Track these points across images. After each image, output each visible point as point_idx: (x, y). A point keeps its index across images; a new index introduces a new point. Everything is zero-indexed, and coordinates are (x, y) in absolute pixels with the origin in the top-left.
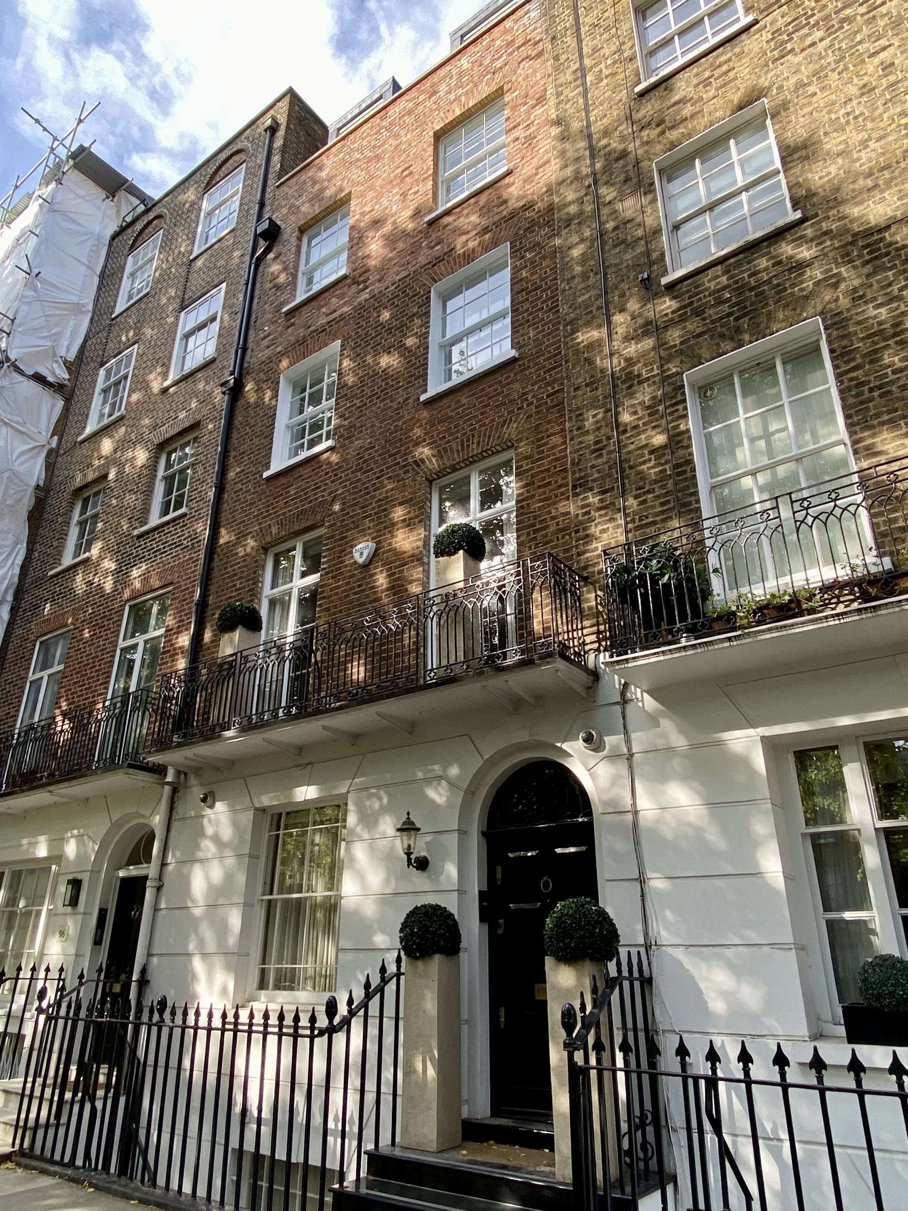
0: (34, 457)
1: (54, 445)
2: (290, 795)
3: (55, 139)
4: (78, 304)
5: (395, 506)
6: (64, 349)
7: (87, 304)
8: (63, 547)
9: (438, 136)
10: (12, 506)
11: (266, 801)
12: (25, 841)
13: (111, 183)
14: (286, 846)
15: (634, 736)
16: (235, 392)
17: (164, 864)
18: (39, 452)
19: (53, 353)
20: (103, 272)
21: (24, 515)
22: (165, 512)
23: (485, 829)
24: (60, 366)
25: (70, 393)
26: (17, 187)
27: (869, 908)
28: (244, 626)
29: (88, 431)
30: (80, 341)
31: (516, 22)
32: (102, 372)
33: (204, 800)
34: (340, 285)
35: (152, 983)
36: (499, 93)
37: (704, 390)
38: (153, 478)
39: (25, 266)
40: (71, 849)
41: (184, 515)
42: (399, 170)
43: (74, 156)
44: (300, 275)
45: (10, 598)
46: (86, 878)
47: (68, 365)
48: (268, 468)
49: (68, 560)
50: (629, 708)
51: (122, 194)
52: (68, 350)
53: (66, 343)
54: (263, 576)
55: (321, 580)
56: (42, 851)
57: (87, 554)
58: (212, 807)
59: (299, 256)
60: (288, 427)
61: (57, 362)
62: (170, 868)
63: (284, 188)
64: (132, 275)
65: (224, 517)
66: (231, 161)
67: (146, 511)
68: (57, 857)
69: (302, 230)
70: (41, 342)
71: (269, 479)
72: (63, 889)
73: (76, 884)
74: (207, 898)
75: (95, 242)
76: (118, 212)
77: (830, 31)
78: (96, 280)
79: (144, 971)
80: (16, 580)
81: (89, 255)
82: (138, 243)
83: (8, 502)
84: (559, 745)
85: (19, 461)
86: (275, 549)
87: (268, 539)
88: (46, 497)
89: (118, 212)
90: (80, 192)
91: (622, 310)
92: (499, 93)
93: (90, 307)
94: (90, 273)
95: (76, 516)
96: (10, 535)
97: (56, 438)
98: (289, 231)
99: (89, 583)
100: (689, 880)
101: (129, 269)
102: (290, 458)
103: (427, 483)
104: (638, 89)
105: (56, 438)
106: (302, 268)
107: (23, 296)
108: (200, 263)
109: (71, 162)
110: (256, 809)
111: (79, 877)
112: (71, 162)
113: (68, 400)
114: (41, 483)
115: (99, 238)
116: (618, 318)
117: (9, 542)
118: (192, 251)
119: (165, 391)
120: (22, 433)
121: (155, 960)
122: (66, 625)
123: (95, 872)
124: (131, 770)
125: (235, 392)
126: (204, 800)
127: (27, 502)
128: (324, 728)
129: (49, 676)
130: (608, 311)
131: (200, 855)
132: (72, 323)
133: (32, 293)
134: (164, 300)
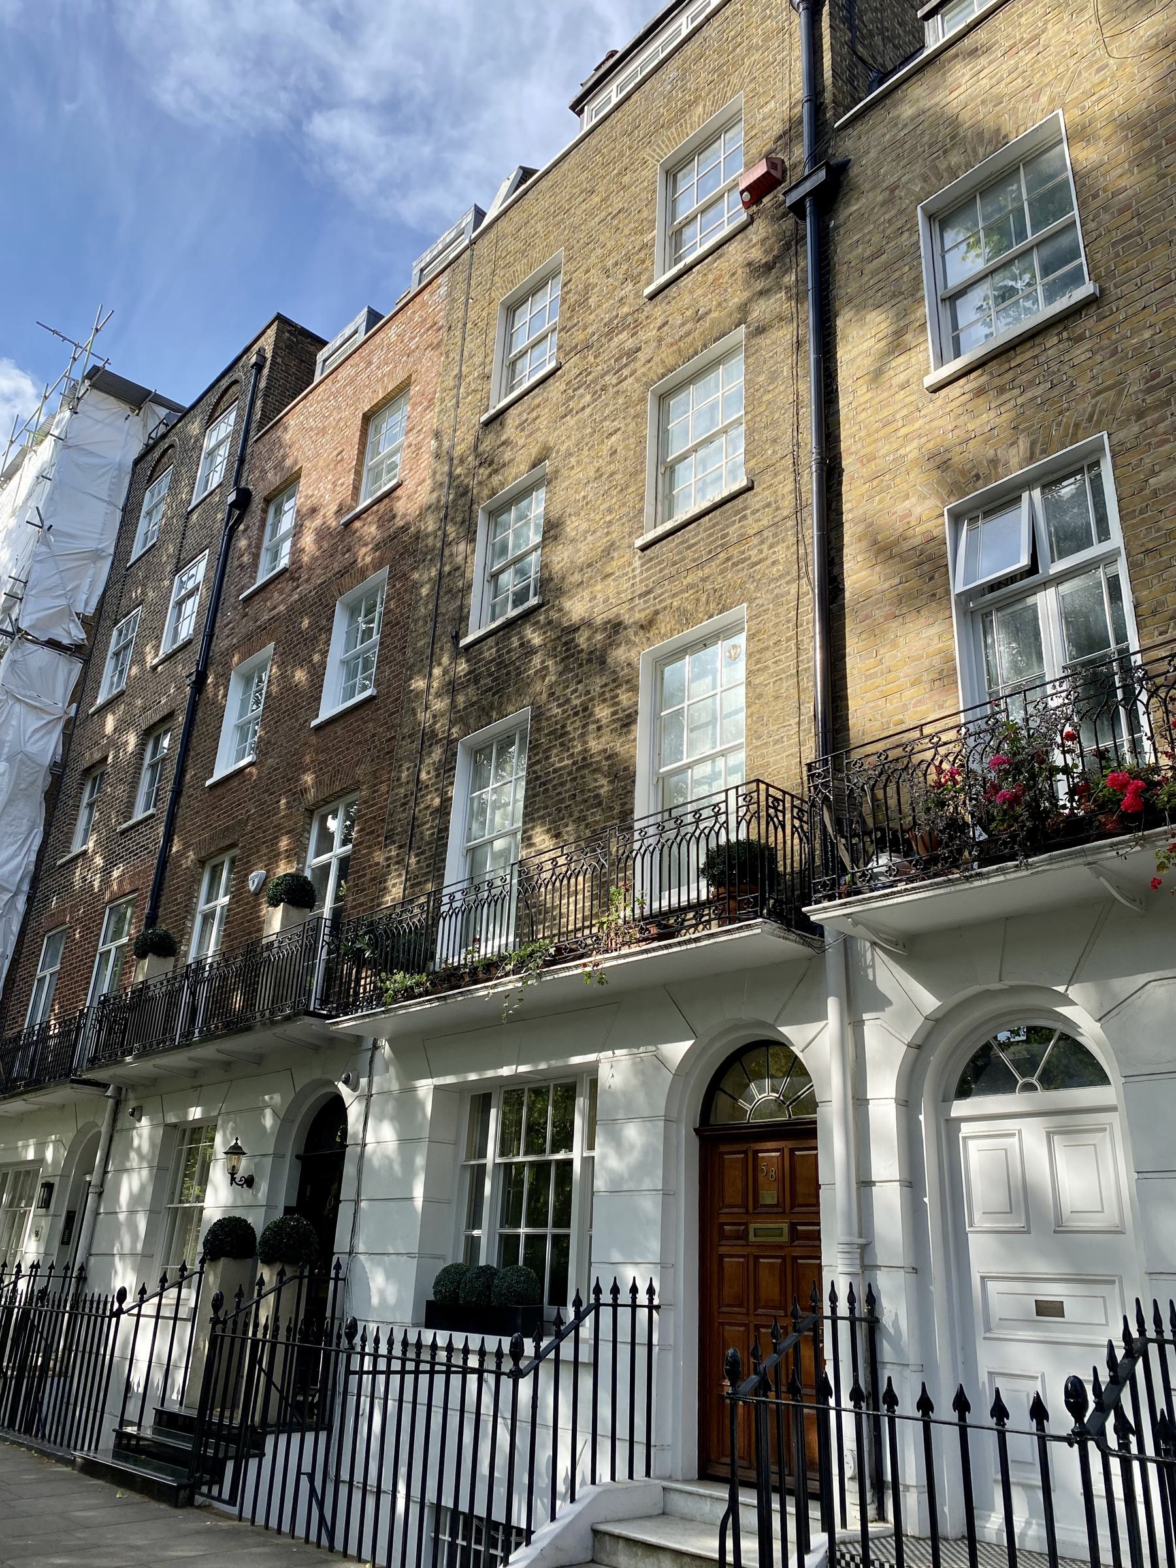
0: (50, 732)
1: (73, 714)
2: (186, 1114)
3: (77, 346)
4: (97, 550)
5: (282, 835)
6: (83, 604)
7: (108, 547)
8: (73, 833)
9: (367, 418)
10: (25, 789)
11: (172, 1119)
12: (20, 1144)
13: (136, 397)
14: (183, 1157)
15: (376, 1079)
16: (199, 684)
17: (105, 1172)
18: (54, 727)
19: (67, 612)
20: (126, 505)
21: (39, 796)
22: (147, 808)
23: (301, 1152)
24: (77, 626)
25: (86, 654)
26: (97, 330)
27: (501, 1235)
28: (154, 954)
29: (100, 701)
30: (100, 591)
31: (432, 294)
32: (115, 633)
33: (132, 1114)
34: (282, 578)
35: (89, 1280)
36: (403, 388)
37: (479, 754)
38: (139, 767)
39: (37, 521)
40: (49, 1154)
41: (152, 816)
42: (335, 453)
43: (89, 376)
44: (263, 551)
45: (26, 887)
46: (56, 1181)
47: (85, 621)
48: (317, 716)
49: (76, 849)
50: (377, 1053)
51: (148, 405)
52: (86, 604)
53: (84, 597)
54: (198, 891)
55: (354, 852)
56: (31, 1155)
57: (84, 848)
58: (139, 1120)
59: (263, 532)
60: (343, 662)
61: (73, 621)
62: (110, 1175)
63: (260, 445)
64: (149, 513)
65: (179, 822)
66: (230, 391)
67: (131, 804)
68: (40, 1161)
69: (268, 501)
70: (57, 602)
71: (319, 728)
72: (39, 1192)
73: (48, 1187)
74: (129, 1205)
75: (116, 473)
76: (145, 426)
77: (596, 396)
78: (119, 514)
79: (82, 1269)
80: (32, 867)
81: (110, 489)
82: (222, 406)
83: (22, 786)
84: (1061, 989)
85: (32, 740)
86: (208, 862)
87: (203, 854)
88: (63, 773)
89: (145, 426)
90: (99, 415)
91: (439, 664)
92: (403, 388)
93: (112, 550)
94: (112, 508)
95: (85, 799)
96: (25, 821)
97: (75, 705)
98: (259, 494)
99: (84, 879)
100: (392, 1204)
101: (145, 508)
102: (344, 701)
103: (307, 814)
104: (483, 419)
105: (75, 705)
106: (266, 543)
107: (36, 555)
108: (195, 516)
109: (87, 383)
110: (167, 1125)
111: (51, 1180)
112: (87, 383)
113: (86, 662)
114: (58, 758)
115: (120, 467)
116: (437, 671)
117: (24, 829)
118: (190, 500)
119: (155, 668)
120: (36, 707)
121: (92, 1260)
122: (65, 923)
123: (64, 1176)
124: (75, 1085)
125: (199, 684)
126: (132, 1114)
127: (42, 782)
128: (190, 1059)
129: (117, 948)
130: (431, 662)
131: (128, 1165)
132: (91, 572)
133: (44, 549)
134: (164, 559)
